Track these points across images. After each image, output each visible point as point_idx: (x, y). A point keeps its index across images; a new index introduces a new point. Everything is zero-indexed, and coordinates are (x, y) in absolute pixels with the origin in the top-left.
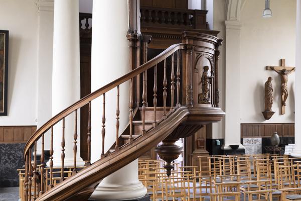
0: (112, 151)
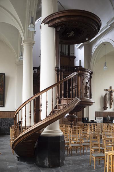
0: (49, 116)
